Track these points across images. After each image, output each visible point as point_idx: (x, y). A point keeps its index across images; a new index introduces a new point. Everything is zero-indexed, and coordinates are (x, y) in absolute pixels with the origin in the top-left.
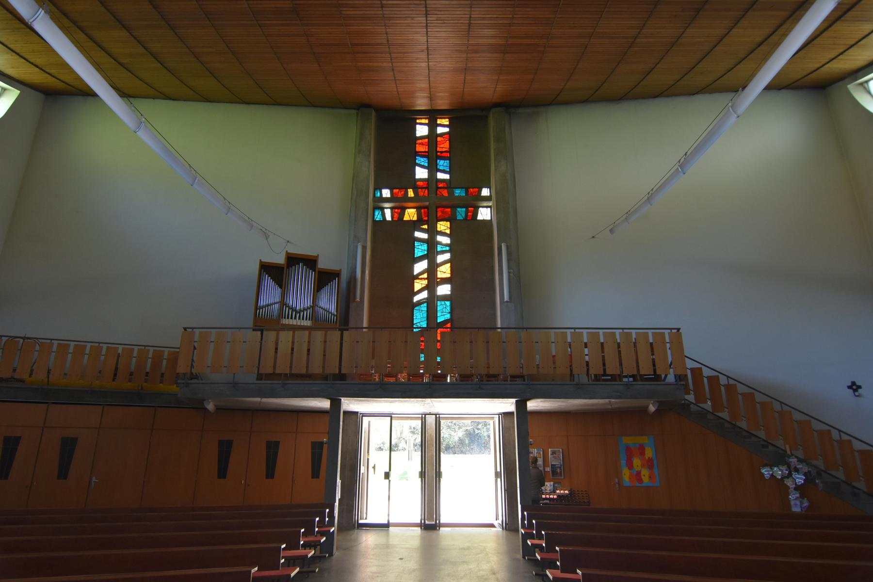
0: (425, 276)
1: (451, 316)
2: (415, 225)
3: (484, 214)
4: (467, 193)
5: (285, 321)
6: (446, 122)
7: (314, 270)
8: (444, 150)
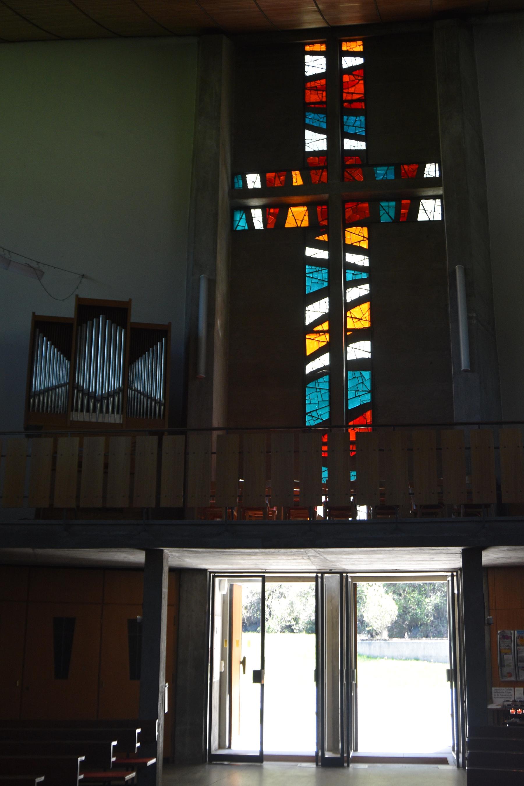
0: (325, 326)
1: (373, 397)
2: (306, 236)
3: (430, 210)
4: (397, 173)
5: (77, 417)
6: (358, 47)
7: (123, 326)
8: (356, 97)
